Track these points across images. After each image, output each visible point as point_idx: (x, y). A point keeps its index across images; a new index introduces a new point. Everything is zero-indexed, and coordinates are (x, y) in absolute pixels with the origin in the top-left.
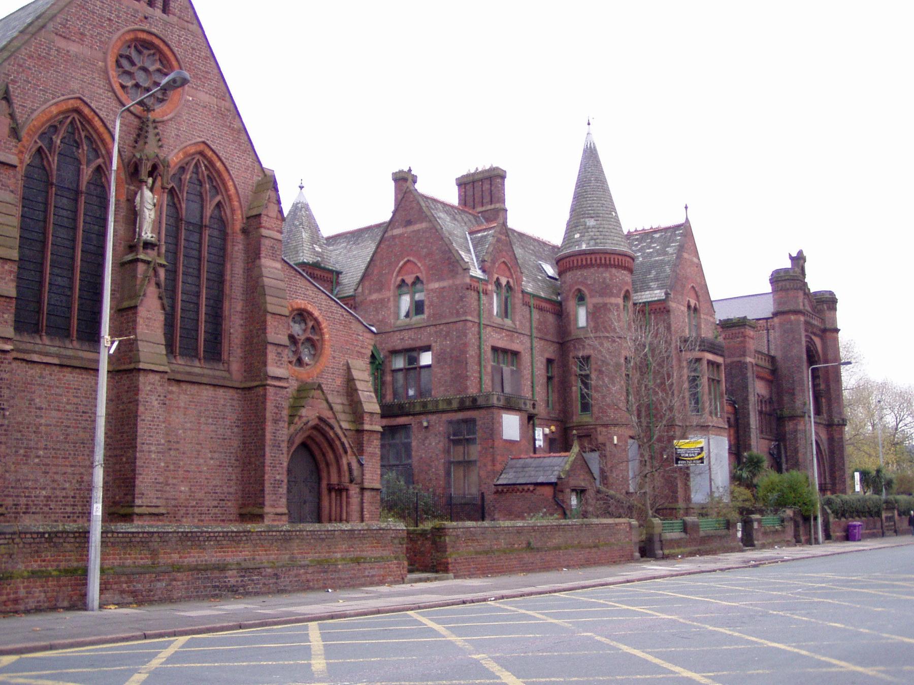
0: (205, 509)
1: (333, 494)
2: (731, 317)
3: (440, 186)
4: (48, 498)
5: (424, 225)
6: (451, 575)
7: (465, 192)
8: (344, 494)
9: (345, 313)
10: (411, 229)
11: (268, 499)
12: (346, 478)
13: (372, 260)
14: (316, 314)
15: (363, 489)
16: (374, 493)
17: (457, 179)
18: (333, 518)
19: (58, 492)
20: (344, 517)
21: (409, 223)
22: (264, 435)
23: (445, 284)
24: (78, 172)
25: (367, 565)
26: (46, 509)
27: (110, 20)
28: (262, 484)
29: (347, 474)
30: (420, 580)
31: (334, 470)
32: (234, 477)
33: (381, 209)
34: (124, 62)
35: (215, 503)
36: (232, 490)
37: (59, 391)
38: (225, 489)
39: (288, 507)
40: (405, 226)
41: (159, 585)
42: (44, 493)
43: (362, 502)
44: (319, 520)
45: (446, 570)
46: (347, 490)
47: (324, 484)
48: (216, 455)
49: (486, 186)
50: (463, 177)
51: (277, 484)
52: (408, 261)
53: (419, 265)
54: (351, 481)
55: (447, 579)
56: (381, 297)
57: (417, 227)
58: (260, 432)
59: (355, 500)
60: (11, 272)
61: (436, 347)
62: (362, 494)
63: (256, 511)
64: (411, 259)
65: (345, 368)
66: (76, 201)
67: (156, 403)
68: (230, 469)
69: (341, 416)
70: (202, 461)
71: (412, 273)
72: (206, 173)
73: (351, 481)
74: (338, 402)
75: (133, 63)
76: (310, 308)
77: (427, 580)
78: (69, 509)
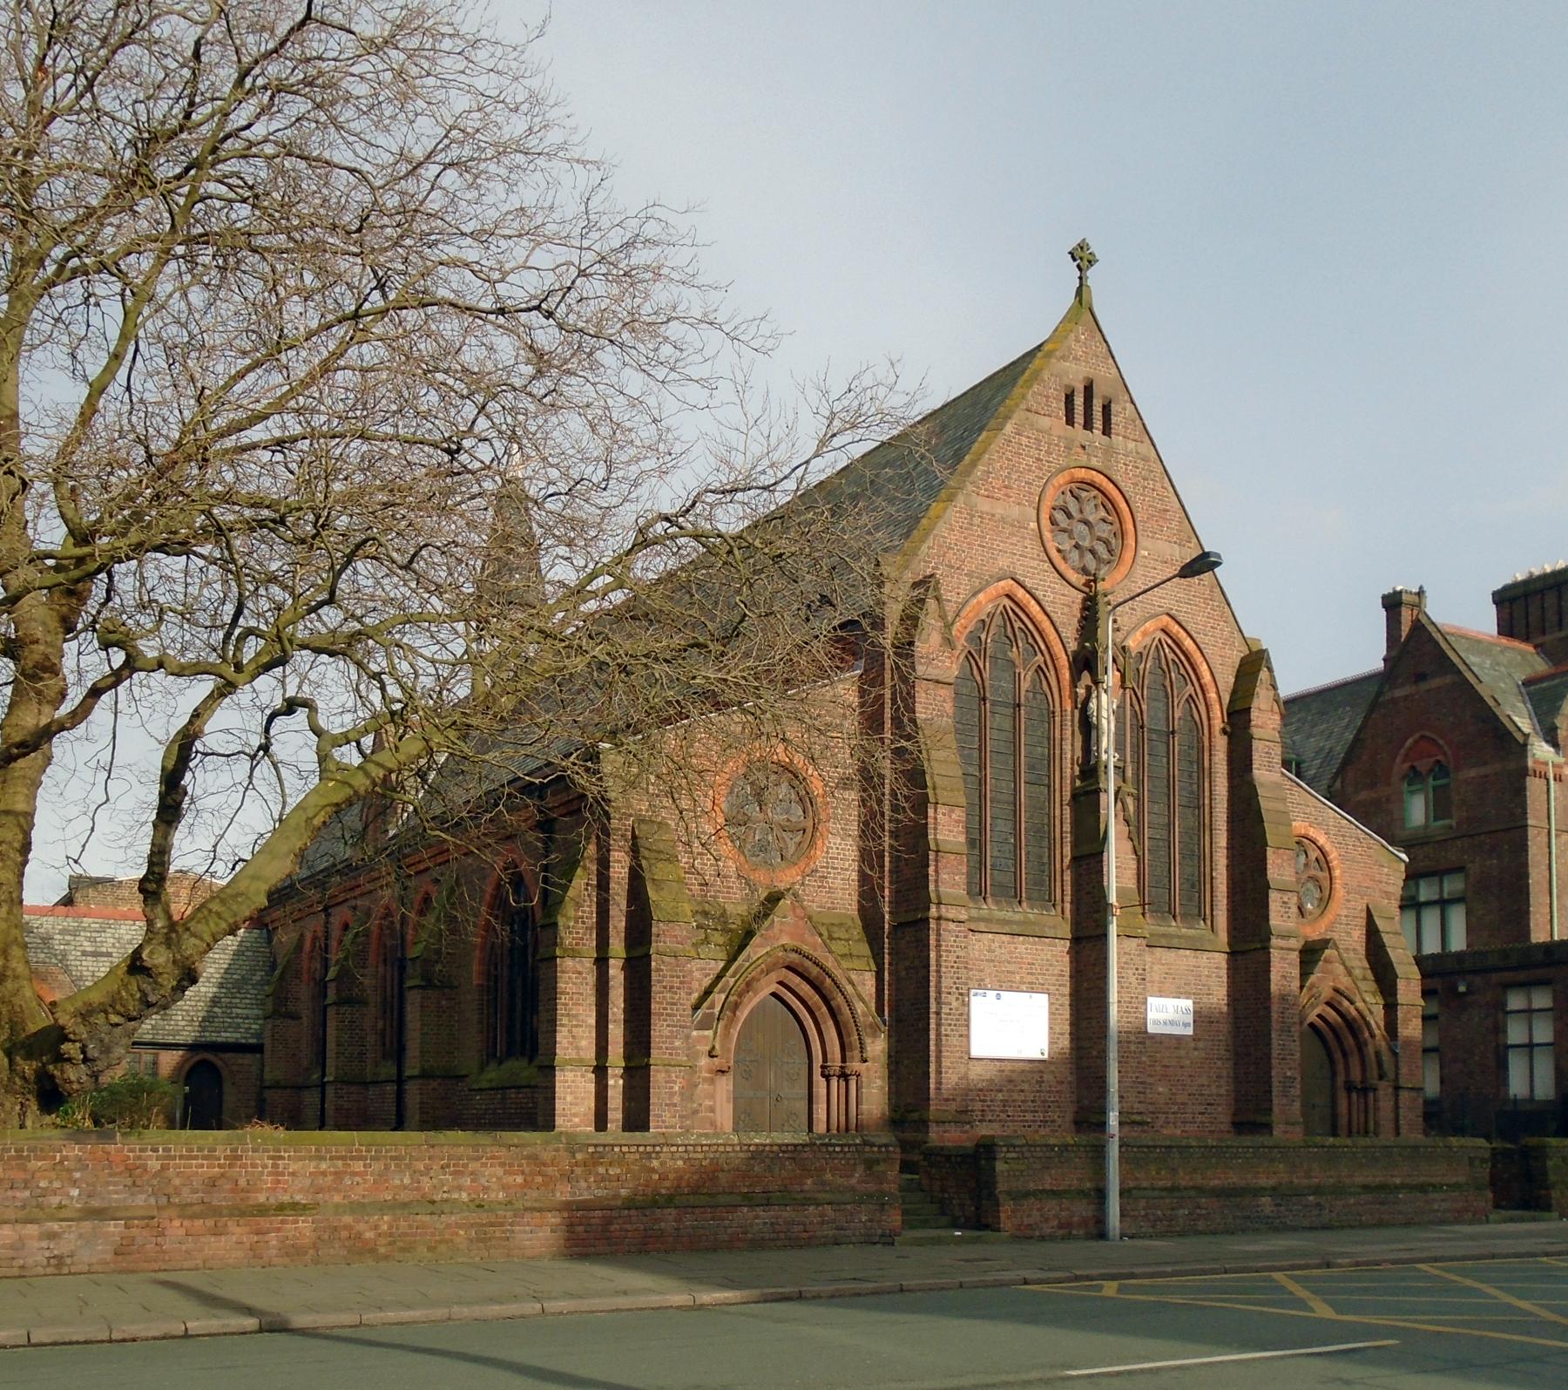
0: (1189, 1117)
1: (1354, 1096)
2: (1537, 572)
3: (1464, 613)
4: (1005, 1102)
5: (1448, 679)
6: (1555, 1214)
7: (1511, 614)
8: (1371, 1095)
9: (1363, 836)
10: (1424, 686)
11: (1277, 1101)
12: (1373, 1071)
13: (1356, 739)
14: (1322, 840)
15: (1397, 1088)
16: (1414, 1094)
17: (1494, 594)
18: (1354, 1130)
19: (1015, 1096)
20: (1371, 1127)
21: (1421, 677)
22: (1269, 1017)
23: (1483, 770)
24: (1016, 679)
25: (1436, 1196)
26: (1003, 1116)
27: (1038, 459)
28: (1269, 1082)
29: (1374, 1066)
30: (1511, 1220)
31: (1354, 1061)
32: (1225, 1073)
33: (1364, 653)
34: (1060, 516)
35: (1202, 1108)
36: (1223, 1091)
37: (1011, 968)
38: (1214, 1090)
39: (1304, 1114)
40: (1416, 682)
41: (1181, 1212)
42: (1000, 1096)
43: (1397, 1107)
44: (1334, 1134)
45: (1548, 1208)
46: (1375, 1090)
47: (1341, 1079)
48: (1201, 1045)
49: (1551, 599)
50: (1506, 588)
51: (1288, 1082)
52: (1423, 737)
53: (1441, 742)
54: (1381, 1077)
55: (1550, 1220)
56: (1374, 795)
57: (1435, 682)
58: (1262, 1013)
59: (1386, 1104)
60: (958, 822)
61: (1474, 868)
62: (1397, 1096)
63: (1263, 1119)
64: (1427, 734)
65: (1364, 914)
66: (1015, 718)
67: (1133, 979)
68: (1219, 1063)
69: (1363, 986)
70: (1182, 1053)
71: (1430, 756)
72: (1171, 656)
73: (1381, 1077)
74: (1359, 963)
75: (1069, 516)
76: (1312, 833)
77: (1522, 1220)
78: (1029, 1117)
